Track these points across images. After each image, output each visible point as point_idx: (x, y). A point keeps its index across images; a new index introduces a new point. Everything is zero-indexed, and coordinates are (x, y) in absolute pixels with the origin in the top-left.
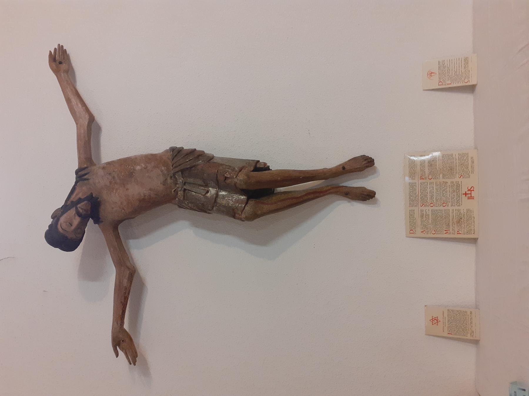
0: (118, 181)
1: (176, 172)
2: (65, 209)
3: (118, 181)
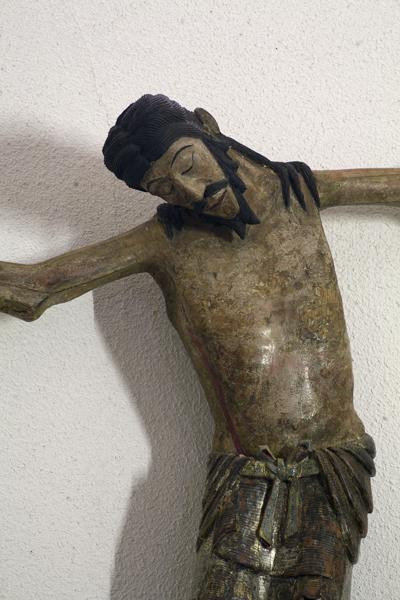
0: (289, 297)
2: (224, 148)
3: (289, 297)
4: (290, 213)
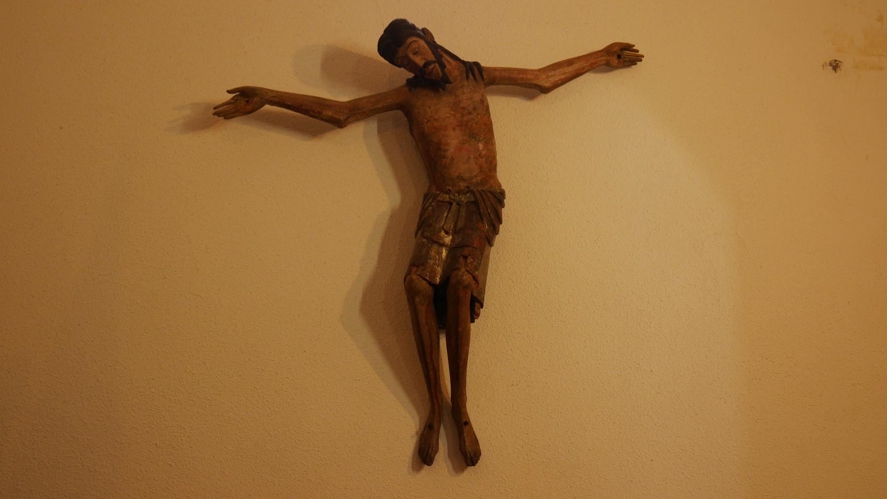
0: (465, 119)
1: (474, 195)
3: (465, 119)
4: (468, 82)
